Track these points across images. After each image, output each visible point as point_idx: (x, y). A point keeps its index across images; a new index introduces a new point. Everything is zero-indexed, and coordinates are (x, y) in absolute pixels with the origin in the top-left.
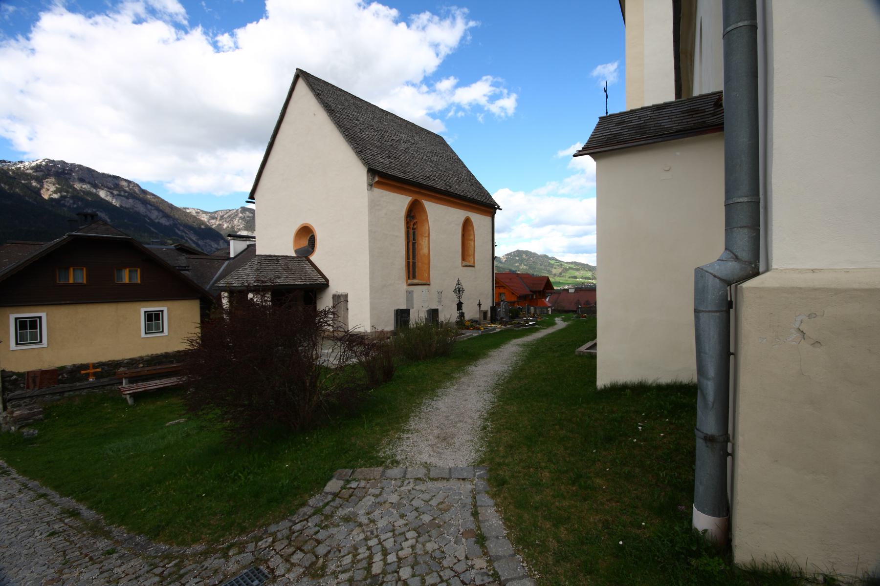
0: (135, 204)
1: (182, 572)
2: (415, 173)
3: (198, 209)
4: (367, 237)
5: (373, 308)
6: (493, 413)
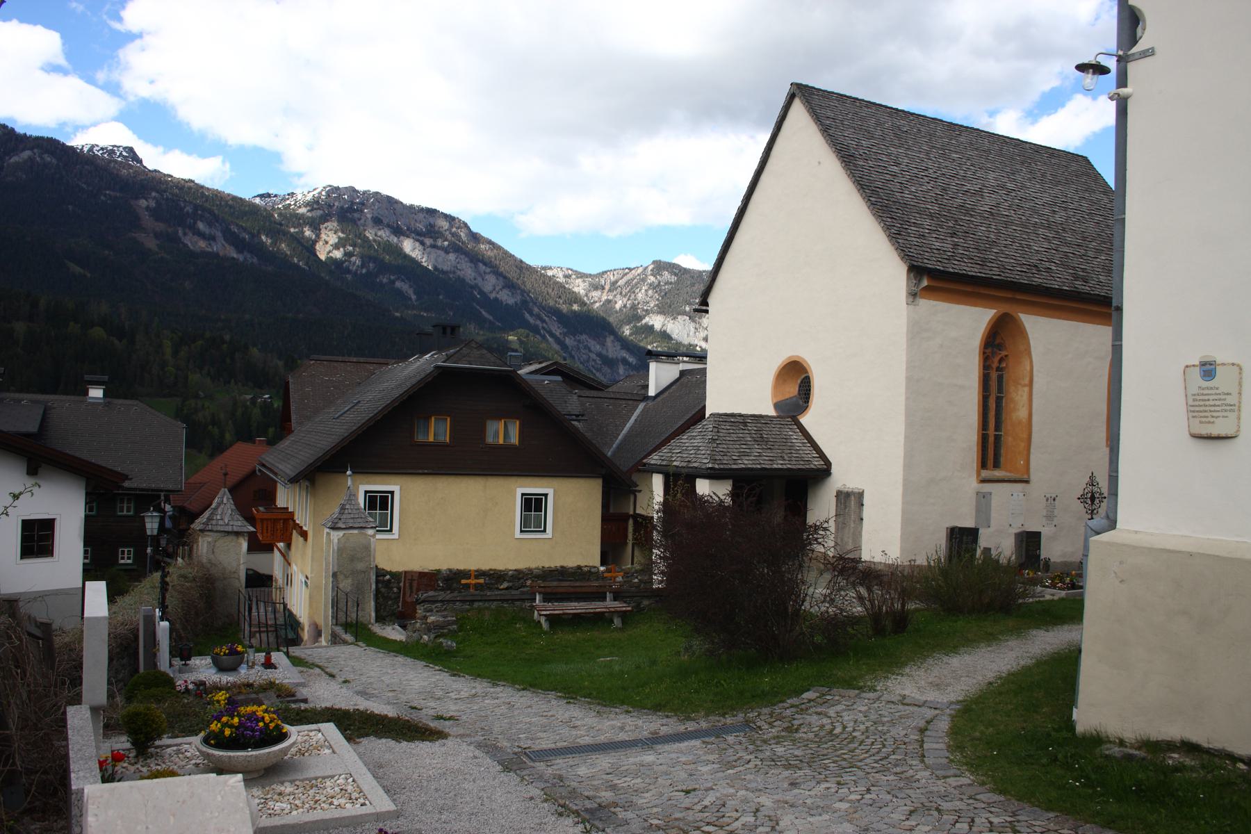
0: (458, 263)
3: (568, 269)
4: (903, 390)
5: (907, 520)
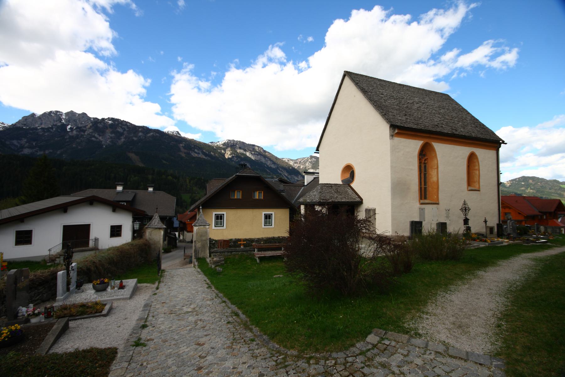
1: (286, 363)
2: (426, 123)
4: (389, 171)
5: (394, 219)
6: (507, 315)
